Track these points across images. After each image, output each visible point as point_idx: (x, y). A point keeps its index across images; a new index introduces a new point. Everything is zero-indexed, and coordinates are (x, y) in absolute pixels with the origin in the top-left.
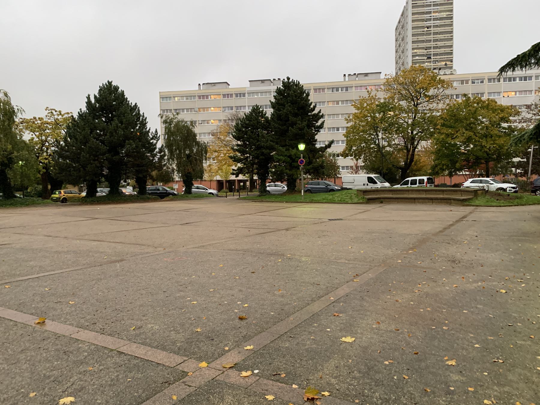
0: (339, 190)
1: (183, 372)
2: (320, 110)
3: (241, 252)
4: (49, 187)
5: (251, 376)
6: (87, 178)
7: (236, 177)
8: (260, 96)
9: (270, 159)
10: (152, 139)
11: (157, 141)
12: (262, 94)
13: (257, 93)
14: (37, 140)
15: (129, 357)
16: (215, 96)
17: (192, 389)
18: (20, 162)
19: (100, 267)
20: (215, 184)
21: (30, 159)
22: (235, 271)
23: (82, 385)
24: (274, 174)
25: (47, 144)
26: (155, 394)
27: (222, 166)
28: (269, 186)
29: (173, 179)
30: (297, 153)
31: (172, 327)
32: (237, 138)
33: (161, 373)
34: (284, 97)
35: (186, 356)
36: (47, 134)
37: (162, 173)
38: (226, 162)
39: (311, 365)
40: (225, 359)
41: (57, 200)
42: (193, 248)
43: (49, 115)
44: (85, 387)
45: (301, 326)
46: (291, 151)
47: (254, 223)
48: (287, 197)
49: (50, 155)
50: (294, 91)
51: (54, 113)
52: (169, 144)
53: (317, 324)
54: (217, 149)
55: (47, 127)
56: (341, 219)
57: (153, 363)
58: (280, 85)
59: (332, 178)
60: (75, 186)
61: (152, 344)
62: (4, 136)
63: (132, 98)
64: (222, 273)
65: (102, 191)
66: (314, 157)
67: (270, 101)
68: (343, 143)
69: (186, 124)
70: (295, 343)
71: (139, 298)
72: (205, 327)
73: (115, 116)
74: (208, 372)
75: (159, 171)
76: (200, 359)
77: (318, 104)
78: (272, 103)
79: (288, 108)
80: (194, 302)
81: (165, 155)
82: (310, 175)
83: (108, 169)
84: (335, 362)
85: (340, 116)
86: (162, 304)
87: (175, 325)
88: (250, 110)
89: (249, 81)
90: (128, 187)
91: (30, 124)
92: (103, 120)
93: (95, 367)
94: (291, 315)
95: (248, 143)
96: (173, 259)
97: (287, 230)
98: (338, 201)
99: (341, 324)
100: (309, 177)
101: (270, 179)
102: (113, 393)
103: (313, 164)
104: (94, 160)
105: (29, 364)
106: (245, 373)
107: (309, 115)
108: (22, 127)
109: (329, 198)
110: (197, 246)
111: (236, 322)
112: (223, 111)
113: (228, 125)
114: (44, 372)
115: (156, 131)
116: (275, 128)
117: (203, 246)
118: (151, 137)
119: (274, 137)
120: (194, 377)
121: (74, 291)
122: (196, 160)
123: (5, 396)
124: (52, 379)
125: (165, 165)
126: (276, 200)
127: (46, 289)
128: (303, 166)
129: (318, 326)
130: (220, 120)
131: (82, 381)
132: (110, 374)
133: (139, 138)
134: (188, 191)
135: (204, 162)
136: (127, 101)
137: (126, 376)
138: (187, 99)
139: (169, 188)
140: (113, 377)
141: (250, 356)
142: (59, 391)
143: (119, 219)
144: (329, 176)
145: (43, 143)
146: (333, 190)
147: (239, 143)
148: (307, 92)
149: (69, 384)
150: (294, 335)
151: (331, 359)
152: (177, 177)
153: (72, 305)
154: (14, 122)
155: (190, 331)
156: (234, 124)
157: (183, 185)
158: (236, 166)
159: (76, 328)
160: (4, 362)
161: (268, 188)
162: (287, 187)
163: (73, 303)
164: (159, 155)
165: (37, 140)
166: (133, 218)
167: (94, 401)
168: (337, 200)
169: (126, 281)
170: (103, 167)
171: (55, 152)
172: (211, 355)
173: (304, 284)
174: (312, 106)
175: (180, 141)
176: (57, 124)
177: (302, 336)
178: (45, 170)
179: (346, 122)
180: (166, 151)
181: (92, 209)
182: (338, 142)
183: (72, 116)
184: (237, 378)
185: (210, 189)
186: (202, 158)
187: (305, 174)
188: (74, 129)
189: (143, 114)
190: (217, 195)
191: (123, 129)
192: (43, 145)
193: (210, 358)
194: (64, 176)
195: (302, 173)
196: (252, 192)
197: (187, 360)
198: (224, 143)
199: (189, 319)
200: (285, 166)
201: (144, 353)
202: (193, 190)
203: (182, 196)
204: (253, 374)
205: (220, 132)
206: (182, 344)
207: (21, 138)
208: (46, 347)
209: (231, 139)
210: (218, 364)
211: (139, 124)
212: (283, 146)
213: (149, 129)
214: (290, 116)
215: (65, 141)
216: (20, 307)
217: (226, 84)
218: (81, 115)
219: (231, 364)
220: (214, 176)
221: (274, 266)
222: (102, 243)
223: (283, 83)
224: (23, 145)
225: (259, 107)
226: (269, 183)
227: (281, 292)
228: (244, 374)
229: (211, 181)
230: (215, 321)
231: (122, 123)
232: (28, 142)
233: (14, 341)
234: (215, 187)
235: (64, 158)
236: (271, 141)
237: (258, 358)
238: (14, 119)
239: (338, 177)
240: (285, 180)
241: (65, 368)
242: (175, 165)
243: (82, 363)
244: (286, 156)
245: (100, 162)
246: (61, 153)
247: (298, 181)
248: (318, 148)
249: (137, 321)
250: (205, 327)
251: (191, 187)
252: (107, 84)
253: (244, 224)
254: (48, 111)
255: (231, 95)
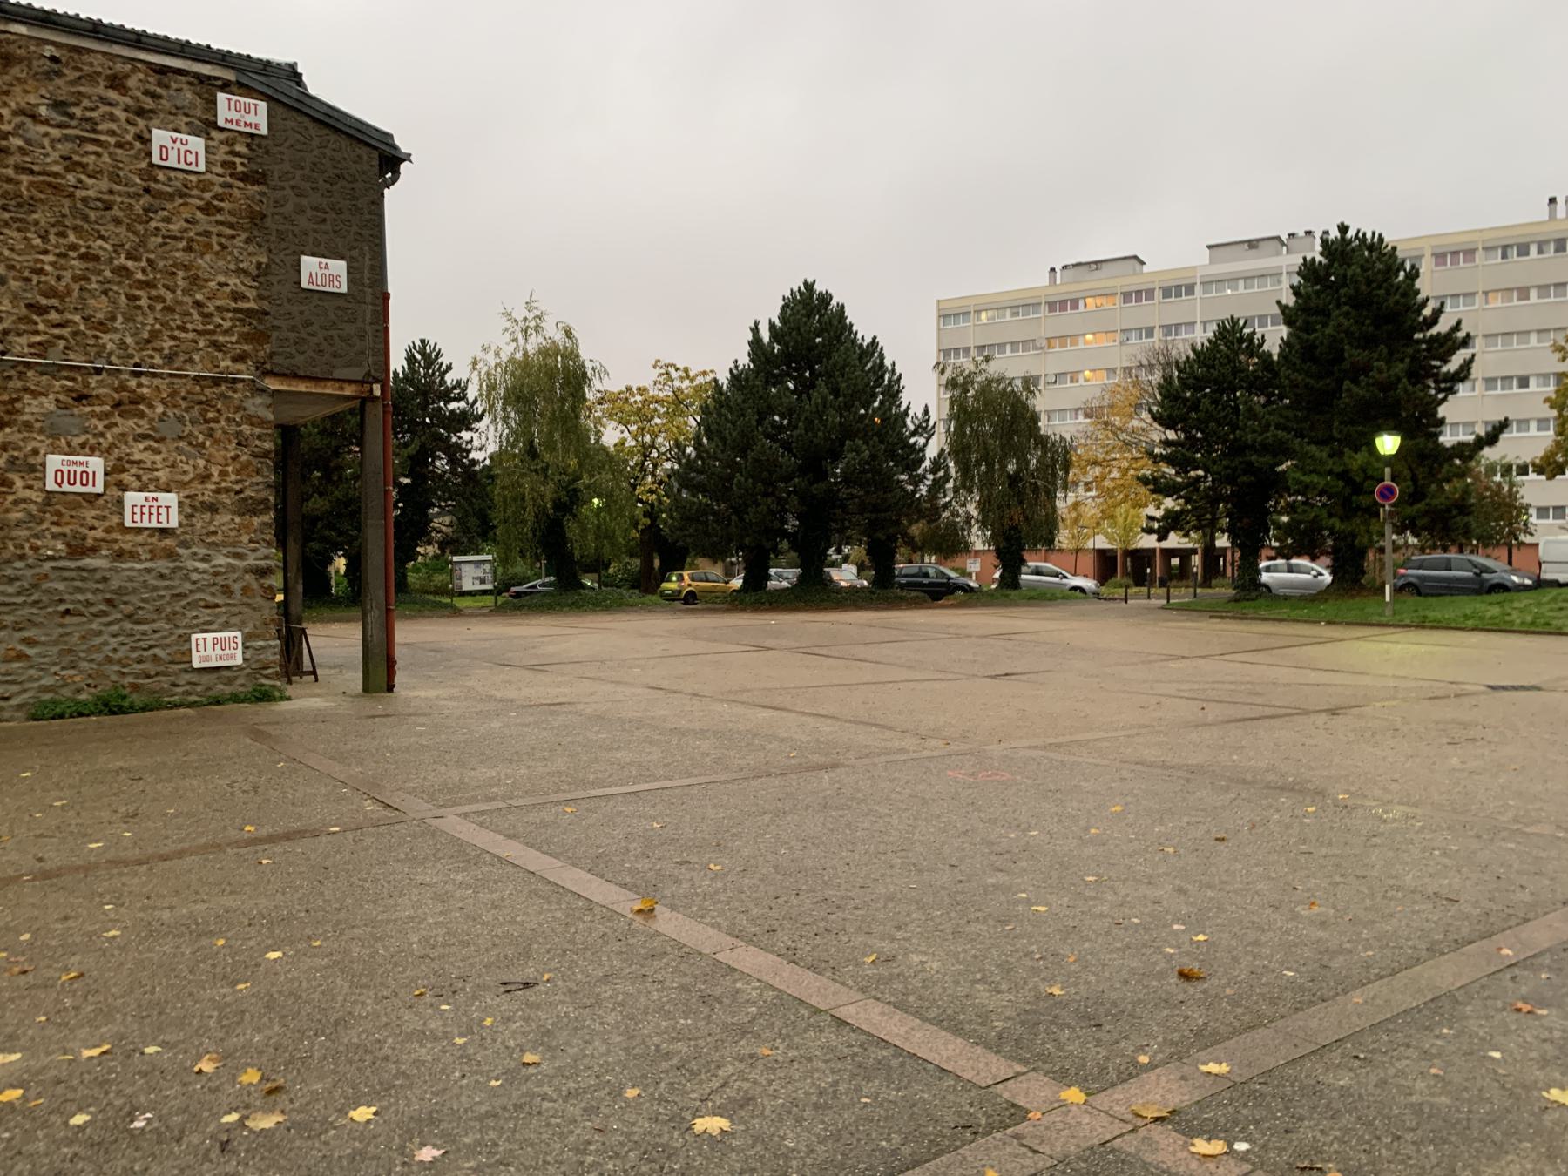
0: (1522, 588)
1: (1014, 1105)
2: (1459, 323)
3: (1179, 773)
4: (657, 563)
5: (1225, 1158)
6: (747, 541)
7: (1159, 540)
8: (1241, 290)
9: (1276, 484)
10: (913, 434)
11: (928, 439)
12: (1248, 282)
13: (1232, 280)
14: (633, 443)
15: (863, 1037)
16: (1099, 301)
17: (1042, 1163)
18: (596, 501)
19: (780, 778)
20: (1088, 562)
21: (617, 492)
22: (1163, 829)
23: (746, 1092)
24: (1287, 530)
25: (655, 454)
26: (936, 1156)
27: (1115, 507)
28: (1268, 569)
29: (967, 545)
30: (1368, 463)
31: (979, 971)
32: (1166, 421)
33: (951, 1097)
34: (1328, 286)
35: (1025, 1062)
36: (656, 430)
37: (938, 527)
38: (1127, 496)
39: (1434, 1161)
40: (1138, 1091)
41: (674, 597)
42: (1030, 747)
43: (661, 379)
44: (753, 1099)
45: (1391, 1026)
46: (1351, 458)
47: (1216, 686)
48: (1328, 608)
49: (660, 483)
50: (1362, 267)
51: (674, 374)
52: (959, 448)
53: (1450, 1028)
54: (1101, 457)
55: (655, 410)
56: (1538, 689)
57: (929, 1066)
58: (1312, 249)
59: (1498, 544)
60: (715, 562)
61: (923, 1011)
62: (562, 436)
63: (864, 326)
64: (1120, 832)
65: (780, 576)
66: (1432, 474)
67: (1278, 303)
68: (1542, 423)
69: (1009, 389)
70: (1373, 1079)
71: (883, 875)
72: (1076, 985)
73: (820, 375)
74: (1087, 1121)
75: (929, 522)
76: (1063, 1077)
77: (1448, 302)
78: (1284, 308)
79: (1341, 318)
80: (1040, 908)
81: (946, 478)
82: (1416, 535)
83: (797, 519)
84: (1523, 1166)
85: (1533, 338)
86: (947, 900)
87: (987, 967)
88: (1211, 335)
89: (1209, 247)
90: (845, 566)
91: (619, 406)
92: (788, 388)
93: (777, 1048)
94: (1354, 988)
95: (1199, 435)
96: (972, 775)
97: (1333, 712)
98: (1523, 623)
99: (1545, 1041)
100: (1412, 540)
101: (1272, 548)
102: (825, 1130)
103: (1427, 500)
104: (766, 495)
105: (621, 1012)
106: (1205, 1143)
107: (1419, 342)
108: (600, 414)
109: (1489, 614)
110: (1035, 742)
111: (1170, 984)
112: (1122, 343)
113: (1136, 384)
114: (656, 1040)
115: (926, 412)
116: (1294, 386)
117: (1059, 745)
118: (912, 427)
119: (1290, 414)
120: (1047, 1128)
121: (720, 836)
122: (1036, 489)
123: (572, 1085)
124: (675, 1061)
125: (946, 506)
126: (1294, 614)
127: (655, 825)
128: (1392, 505)
129: (1455, 1037)
130: (1111, 371)
131: (747, 1080)
132: (816, 1075)
133: (878, 434)
134: (1010, 581)
135: (1058, 494)
136: (851, 331)
137: (858, 1089)
138: (1015, 314)
139: (954, 569)
140: (823, 1085)
141: (1219, 1093)
142: (694, 1096)
143: (824, 651)
144: (1487, 541)
145: (645, 451)
146: (1502, 588)
147: (1171, 435)
148: (1408, 267)
149: (715, 1084)
150: (1371, 1052)
151: (1507, 1153)
152: (978, 539)
153: (716, 873)
154: (585, 400)
155: (1030, 990)
156: (1157, 378)
157: (997, 562)
158: (1158, 507)
159: (728, 938)
160: (568, 999)
161: (1265, 577)
162: (1333, 573)
163: (718, 868)
164: (931, 477)
165: (633, 443)
166: (860, 651)
167: (776, 1139)
168: (1518, 621)
169: (849, 825)
170: (786, 511)
171: (672, 474)
172: (1095, 1071)
173: (1400, 895)
174: (1427, 312)
175: (992, 436)
176: (678, 400)
177: (1399, 1059)
178: (648, 521)
179: (1558, 355)
180: (951, 465)
181: (747, 622)
182: (1523, 426)
183: (716, 380)
184: (1180, 1155)
185: (1075, 574)
186: (1054, 484)
187: (1399, 534)
188: (720, 415)
189: (894, 364)
190: (1097, 595)
191: (839, 410)
192: (646, 457)
193: (1096, 1081)
194: (690, 535)
195: (1388, 529)
196: (1210, 587)
197: (1024, 1074)
198: (1124, 436)
199: (1026, 955)
200: (1324, 505)
201: (902, 1033)
202: (1023, 576)
203: (991, 594)
204: (1231, 1152)
205: (1111, 406)
206: (1010, 1023)
207: (597, 441)
208: (658, 976)
209: (1145, 426)
210: (1117, 1099)
211: (882, 393)
212: (1320, 443)
213: (908, 408)
214: (1346, 347)
215: (698, 446)
216: (599, 866)
217: (1134, 262)
218: (735, 378)
219: (1159, 1110)
220: (1087, 537)
221: (1288, 827)
222: (784, 714)
223: (1325, 242)
224: (602, 457)
225: (1241, 323)
226: (1270, 558)
227: (1316, 909)
228: (1202, 1146)
229: (1077, 551)
230: (1103, 971)
231: (836, 392)
232: (612, 449)
233: (586, 948)
234: (1091, 570)
235: (695, 488)
236: (1278, 427)
237: (1245, 1106)
238: (584, 392)
239: (1523, 543)
240: (1325, 553)
241: (704, 1038)
242: (974, 505)
243: (744, 1033)
244: (1330, 472)
245: (779, 499)
246: (687, 476)
247: (1371, 555)
248: (1448, 445)
249: (883, 939)
250: (1076, 985)
251: (1019, 568)
252: (802, 289)
253: (1185, 687)
254: (659, 371)
255: (1150, 294)
